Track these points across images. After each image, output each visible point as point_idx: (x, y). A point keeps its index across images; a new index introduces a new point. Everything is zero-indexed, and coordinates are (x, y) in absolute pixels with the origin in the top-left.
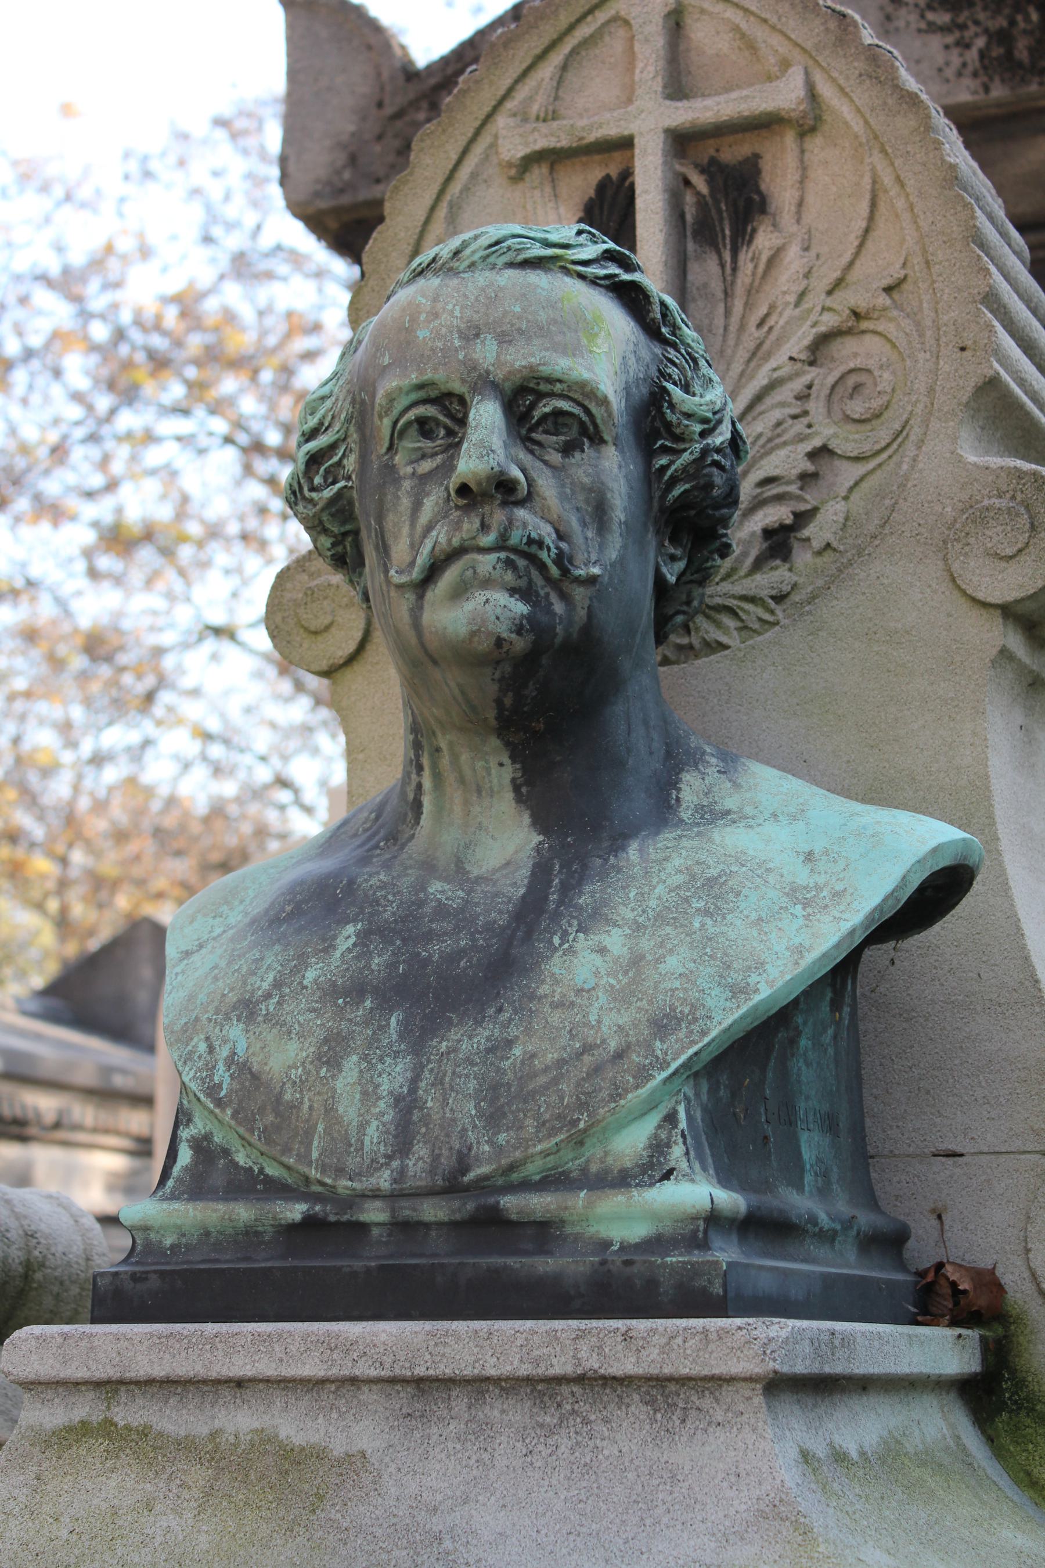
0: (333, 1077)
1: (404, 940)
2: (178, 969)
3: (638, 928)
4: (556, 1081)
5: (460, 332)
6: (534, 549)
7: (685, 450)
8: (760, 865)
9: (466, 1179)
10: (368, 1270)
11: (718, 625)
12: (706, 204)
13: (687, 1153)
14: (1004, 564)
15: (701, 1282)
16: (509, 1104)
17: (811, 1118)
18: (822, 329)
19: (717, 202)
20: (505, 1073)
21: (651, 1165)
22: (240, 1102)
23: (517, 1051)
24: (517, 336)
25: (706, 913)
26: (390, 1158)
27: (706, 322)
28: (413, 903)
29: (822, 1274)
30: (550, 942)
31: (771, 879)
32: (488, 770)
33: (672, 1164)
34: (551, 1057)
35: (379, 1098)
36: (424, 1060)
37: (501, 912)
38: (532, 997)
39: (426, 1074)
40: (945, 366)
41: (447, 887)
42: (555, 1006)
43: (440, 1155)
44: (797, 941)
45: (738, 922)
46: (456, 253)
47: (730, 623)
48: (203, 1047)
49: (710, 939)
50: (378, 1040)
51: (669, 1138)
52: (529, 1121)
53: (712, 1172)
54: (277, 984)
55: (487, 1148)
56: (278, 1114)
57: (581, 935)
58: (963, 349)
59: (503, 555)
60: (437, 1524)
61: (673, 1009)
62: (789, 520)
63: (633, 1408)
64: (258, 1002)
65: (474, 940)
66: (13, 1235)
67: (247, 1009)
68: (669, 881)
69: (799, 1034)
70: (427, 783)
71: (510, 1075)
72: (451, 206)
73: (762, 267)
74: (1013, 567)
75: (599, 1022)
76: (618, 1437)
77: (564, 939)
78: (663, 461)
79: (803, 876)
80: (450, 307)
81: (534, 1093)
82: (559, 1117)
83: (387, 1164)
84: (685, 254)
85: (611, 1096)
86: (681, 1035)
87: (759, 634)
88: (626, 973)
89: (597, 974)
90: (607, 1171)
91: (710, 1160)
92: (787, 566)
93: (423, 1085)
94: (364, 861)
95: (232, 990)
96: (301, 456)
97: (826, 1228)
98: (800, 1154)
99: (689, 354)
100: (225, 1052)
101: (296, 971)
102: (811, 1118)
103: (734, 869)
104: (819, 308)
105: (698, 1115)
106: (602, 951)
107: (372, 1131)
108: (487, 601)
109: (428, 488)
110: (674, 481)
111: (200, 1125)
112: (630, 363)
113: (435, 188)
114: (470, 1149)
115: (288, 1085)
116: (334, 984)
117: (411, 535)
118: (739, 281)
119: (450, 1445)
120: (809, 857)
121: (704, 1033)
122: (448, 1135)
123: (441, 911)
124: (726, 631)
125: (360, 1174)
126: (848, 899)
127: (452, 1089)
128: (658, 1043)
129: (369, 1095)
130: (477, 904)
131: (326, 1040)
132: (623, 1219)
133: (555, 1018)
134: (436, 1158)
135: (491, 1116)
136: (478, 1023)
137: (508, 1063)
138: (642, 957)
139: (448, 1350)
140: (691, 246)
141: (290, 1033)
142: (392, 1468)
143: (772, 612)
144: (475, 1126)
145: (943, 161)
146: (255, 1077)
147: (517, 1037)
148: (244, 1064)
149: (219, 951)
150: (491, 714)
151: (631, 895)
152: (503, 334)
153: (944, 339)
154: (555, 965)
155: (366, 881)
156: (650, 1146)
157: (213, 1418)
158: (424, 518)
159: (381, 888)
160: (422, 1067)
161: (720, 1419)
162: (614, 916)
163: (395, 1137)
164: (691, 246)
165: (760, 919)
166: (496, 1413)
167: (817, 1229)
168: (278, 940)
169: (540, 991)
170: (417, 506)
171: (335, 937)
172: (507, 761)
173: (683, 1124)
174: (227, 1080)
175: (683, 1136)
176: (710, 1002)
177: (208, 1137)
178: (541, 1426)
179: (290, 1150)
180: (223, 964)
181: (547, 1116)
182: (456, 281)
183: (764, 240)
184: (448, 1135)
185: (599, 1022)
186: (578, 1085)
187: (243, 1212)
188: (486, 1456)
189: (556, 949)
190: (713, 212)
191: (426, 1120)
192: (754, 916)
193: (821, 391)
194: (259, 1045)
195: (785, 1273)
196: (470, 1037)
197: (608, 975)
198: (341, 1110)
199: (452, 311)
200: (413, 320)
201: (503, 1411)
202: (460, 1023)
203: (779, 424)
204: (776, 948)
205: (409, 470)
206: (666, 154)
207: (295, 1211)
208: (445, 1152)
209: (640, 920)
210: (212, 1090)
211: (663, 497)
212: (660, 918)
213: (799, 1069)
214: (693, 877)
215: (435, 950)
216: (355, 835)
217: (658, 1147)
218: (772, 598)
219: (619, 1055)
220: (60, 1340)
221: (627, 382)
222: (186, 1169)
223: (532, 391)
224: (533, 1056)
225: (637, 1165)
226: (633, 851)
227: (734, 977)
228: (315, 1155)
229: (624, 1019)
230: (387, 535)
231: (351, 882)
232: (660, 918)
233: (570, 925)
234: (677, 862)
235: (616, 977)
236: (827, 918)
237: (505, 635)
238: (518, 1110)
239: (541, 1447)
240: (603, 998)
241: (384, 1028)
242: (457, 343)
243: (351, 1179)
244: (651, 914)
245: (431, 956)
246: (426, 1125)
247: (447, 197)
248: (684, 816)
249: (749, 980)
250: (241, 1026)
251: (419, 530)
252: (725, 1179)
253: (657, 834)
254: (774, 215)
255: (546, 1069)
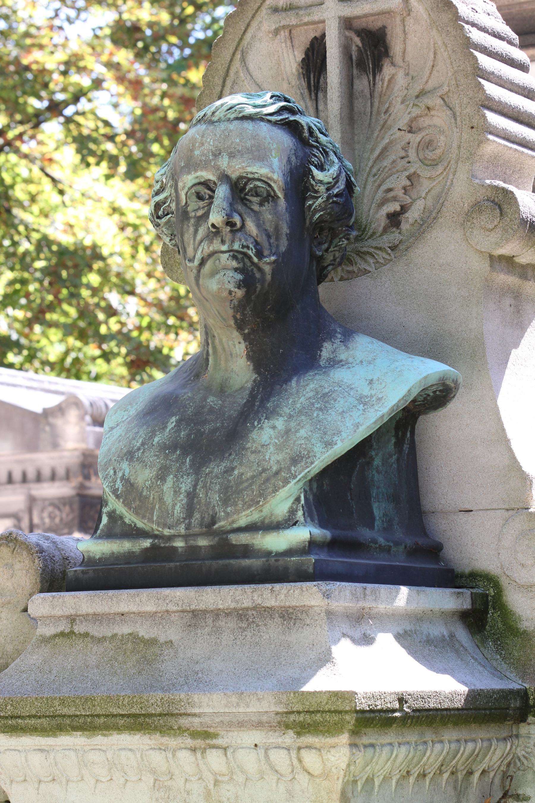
0: (163, 484)
1: (195, 424)
2: (107, 436)
3: (290, 416)
4: (251, 485)
5: (212, 152)
6: (245, 250)
7: (320, 197)
8: (348, 387)
9: (215, 527)
10: (176, 566)
11: (366, 261)
12: (361, 51)
13: (304, 514)
14: (488, 233)
15: (305, 567)
16: (232, 495)
17: (381, 496)
18: (414, 115)
19: (366, 51)
20: (230, 482)
21: (289, 520)
22: (126, 496)
23: (236, 472)
24: (237, 153)
25: (321, 409)
26: (185, 519)
27: (363, 109)
28: (200, 407)
29: (375, 565)
30: (253, 424)
31: (352, 393)
32: (234, 345)
33: (298, 519)
34: (249, 474)
35: (181, 494)
36: (199, 477)
37: (235, 411)
38: (244, 449)
39: (200, 483)
40: (465, 136)
41: (215, 399)
42: (253, 452)
43: (204, 517)
44: (357, 421)
45: (333, 413)
46: (214, 113)
47: (371, 261)
48: (112, 472)
49: (319, 421)
50: (181, 468)
51: (297, 507)
52: (240, 502)
53: (316, 522)
54: (143, 444)
55: (223, 514)
56: (140, 501)
57: (266, 421)
58: (472, 128)
59: (231, 254)
60: (197, 668)
61: (300, 452)
62: (398, 208)
63: (276, 620)
64: (135, 452)
65: (223, 424)
66: (57, 558)
67: (130, 455)
68: (307, 395)
69: (373, 460)
70: (211, 351)
71: (233, 483)
72: (243, 52)
73: (386, 83)
74: (493, 234)
75: (270, 459)
76: (269, 631)
77: (259, 423)
78: (310, 202)
79: (366, 391)
80: (209, 140)
81: (242, 490)
82: (252, 500)
83: (183, 522)
84: (352, 75)
85: (273, 490)
86: (303, 464)
87: (385, 265)
88: (283, 437)
89: (271, 438)
90: (272, 522)
91: (316, 517)
92: (399, 231)
93: (198, 487)
94: (184, 386)
95: (125, 447)
96: (153, 203)
97: (383, 545)
98: (372, 513)
99: (324, 150)
100: (120, 475)
101: (151, 438)
102: (381, 496)
103: (336, 389)
104: (411, 105)
105: (311, 497)
106: (274, 427)
107: (178, 508)
108: (225, 274)
109: (200, 223)
110: (316, 211)
111: (111, 506)
112: (292, 159)
113: (235, 44)
114: (216, 514)
115: (145, 489)
116: (165, 444)
117: (194, 244)
118: (376, 90)
119: (205, 637)
120: (371, 382)
121: (312, 463)
122: (207, 509)
123: (211, 410)
124: (369, 265)
125: (173, 526)
126: (383, 401)
127: (210, 489)
128: (293, 468)
129: (177, 492)
130: (226, 407)
131: (160, 469)
132: (277, 542)
133: (252, 457)
134: (203, 518)
135: (225, 500)
136: (222, 460)
137: (232, 477)
138: (290, 430)
139: (203, 598)
140: (355, 72)
141: (146, 466)
142: (182, 648)
143: (389, 254)
144: (218, 505)
145: (464, 35)
146: (132, 485)
147: (236, 466)
148: (128, 479)
149: (123, 428)
150: (232, 322)
151: (290, 402)
152: (231, 153)
153: (464, 122)
154: (254, 435)
155: (183, 396)
156: (289, 511)
157: (113, 629)
158: (199, 237)
159: (188, 400)
160: (199, 479)
161: (308, 622)
162: (281, 412)
163: (187, 510)
164: (355, 72)
165: (343, 412)
166: (223, 623)
167: (377, 546)
168: (146, 424)
169: (247, 446)
170: (196, 231)
171: (167, 423)
172: (242, 341)
173: (303, 502)
174: (121, 487)
175: (303, 507)
176: (316, 449)
177: (114, 511)
178: (241, 628)
179: (145, 516)
180: (123, 435)
181: (247, 500)
182: (212, 127)
183: (387, 70)
184: (207, 509)
185: (270, 459)
186: (260, 486)
187: (125, 546)
188: (218, 641)
189: (255, 427)
190: (364, 55)
191: (199, 503)
192: (341, 410)
193: (414, 145)
194: (134, 471)
195: (351, 564)
196: (218, 467)
197: (275, 438)
198: (165, 499)
199: (209, 142)
200: (193, 146)
201: (226, 623)
202: (214, 460)
203: (394, 161)
204: (348, 425)
205: (193, 214)
206: (340, 28)
207: (147, 543)
208: (206, 516)
209: (292, 413)
210: (115, 492)
211: (312, 218)
212: (300, 412)
213: (373, 475)
214: (317, 393)
215: (207, 428)
216: (186, 372)
217: (292, 512)
218: (389, 247)
219: (277, 473)
220: (51, 599)
221: (291, 169)
222: (105, 525)
223: (245, 177)
224: (242, 474)
225: (284, 520)
226: (294, 383)
227: (327, 438)
228: (155, 518)
229: (280, 457)
230: (185, 243)
231: (177, 397)
232: (300, 412)
233: (262, 416)
234: (312, 386)
235: (278, 439)
236: (372, 410)
237: (232, 289)
238: (235, 497)
239: (240, 636)
240: (272, 449)
241: (184, 463)
242: (211, 157)
243: (169, 528)
244: (297, 410)
245: (205, 431)
246: (199, 505)
247: (240, 48)
248: (321, 363)
249: (334, 439)
250: (127, 463)
251: (197, 242)
252: (322, 525)
253: (306, 373)
254: (392, 57)
255: (248, 480)
